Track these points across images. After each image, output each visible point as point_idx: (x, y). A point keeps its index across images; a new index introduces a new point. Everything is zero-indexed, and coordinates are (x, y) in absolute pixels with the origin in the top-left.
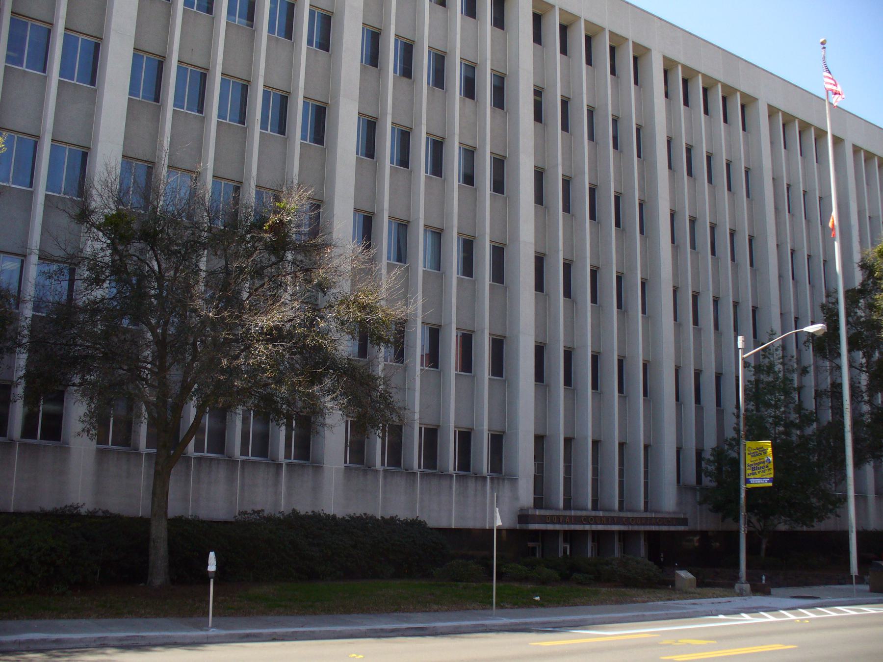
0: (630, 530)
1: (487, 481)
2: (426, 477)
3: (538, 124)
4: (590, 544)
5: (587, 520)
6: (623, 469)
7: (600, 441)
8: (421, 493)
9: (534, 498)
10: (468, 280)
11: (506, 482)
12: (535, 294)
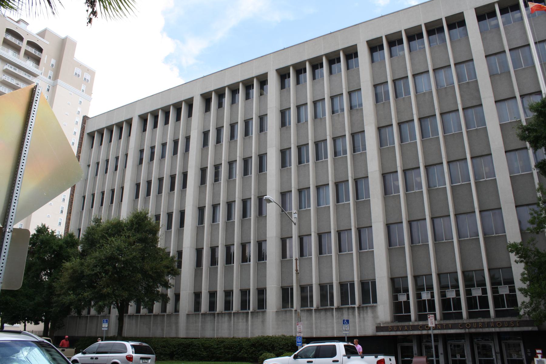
5: (414, 328)
8: (316, 319)
11: (368, 308)
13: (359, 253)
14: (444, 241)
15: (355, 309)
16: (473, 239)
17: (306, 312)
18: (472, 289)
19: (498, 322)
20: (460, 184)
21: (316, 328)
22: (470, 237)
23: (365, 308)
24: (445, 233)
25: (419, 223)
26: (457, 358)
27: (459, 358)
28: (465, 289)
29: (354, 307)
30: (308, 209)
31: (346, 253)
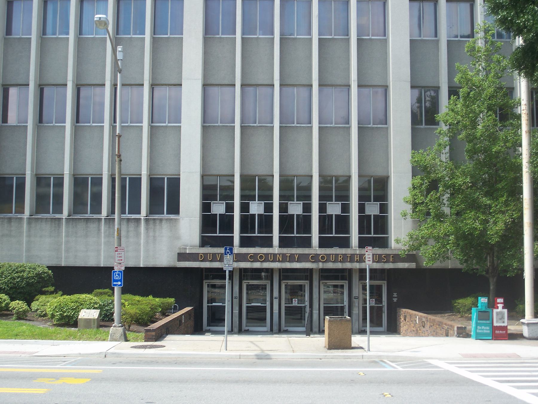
1: (141, 222)
8: (67, 236)
11: (164, 222)
13: (75, 126)
14: (295, 125)
16: (340, 127)
17: (49, 223)
18: (366, 204)
19: (322, 254)
20: (330, 37)
21: (67, 251)
22: (335, 124)
23: (158, 222)
25: (259, 90)
26: (293, 304)
27: (297, 304)
28: (312, 202)
29: (60, 219)
30: (59, 36)
31: (127, 124)
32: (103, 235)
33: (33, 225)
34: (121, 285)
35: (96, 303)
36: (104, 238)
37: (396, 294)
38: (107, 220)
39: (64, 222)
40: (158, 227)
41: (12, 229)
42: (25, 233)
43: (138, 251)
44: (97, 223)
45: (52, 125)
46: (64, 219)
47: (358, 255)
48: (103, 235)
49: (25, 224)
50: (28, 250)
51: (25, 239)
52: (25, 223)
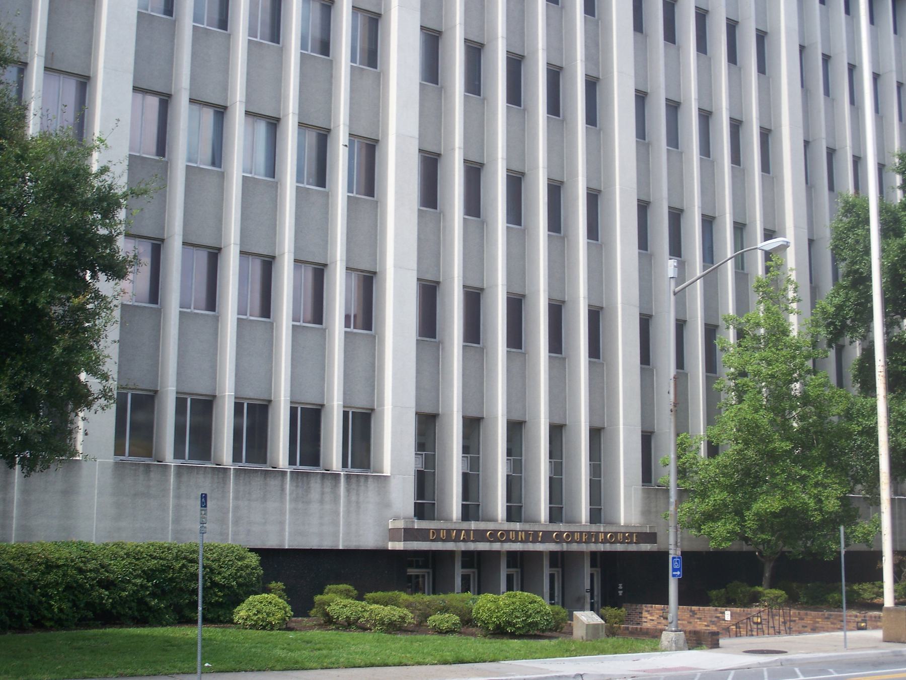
0: (565, 550)
1: (340, 479)
2: (243, 475)
3: (638, 34)
4: (547, 571)
6: (600, 464)
7: (525, 422)
8: (236, 498)
9: (590, 509)
10: (517, 229)
12: (639, 253)
15: (339, 480)
17: (210, 475)
21: (236, 522)
23: (362, 480)
24: (304, 312)
32: (288, 498)
33: (185, 478)
34: (679, 576)
35: (777, 598)
36: (291, 501)
37: (280, 585)
38: (295, 475)
39: (232, 475)
40: (362, 488)
41: (151, 483)
42: (171, 491)
43: (336, 524)
44: (280, 478)
45: (189, 310)
46: (232, 470)
47: (445, 531)
48: (288, 498)
49: (172, 477)
50: (177, 521)
51: (171, 502)
52: (172, 474)
